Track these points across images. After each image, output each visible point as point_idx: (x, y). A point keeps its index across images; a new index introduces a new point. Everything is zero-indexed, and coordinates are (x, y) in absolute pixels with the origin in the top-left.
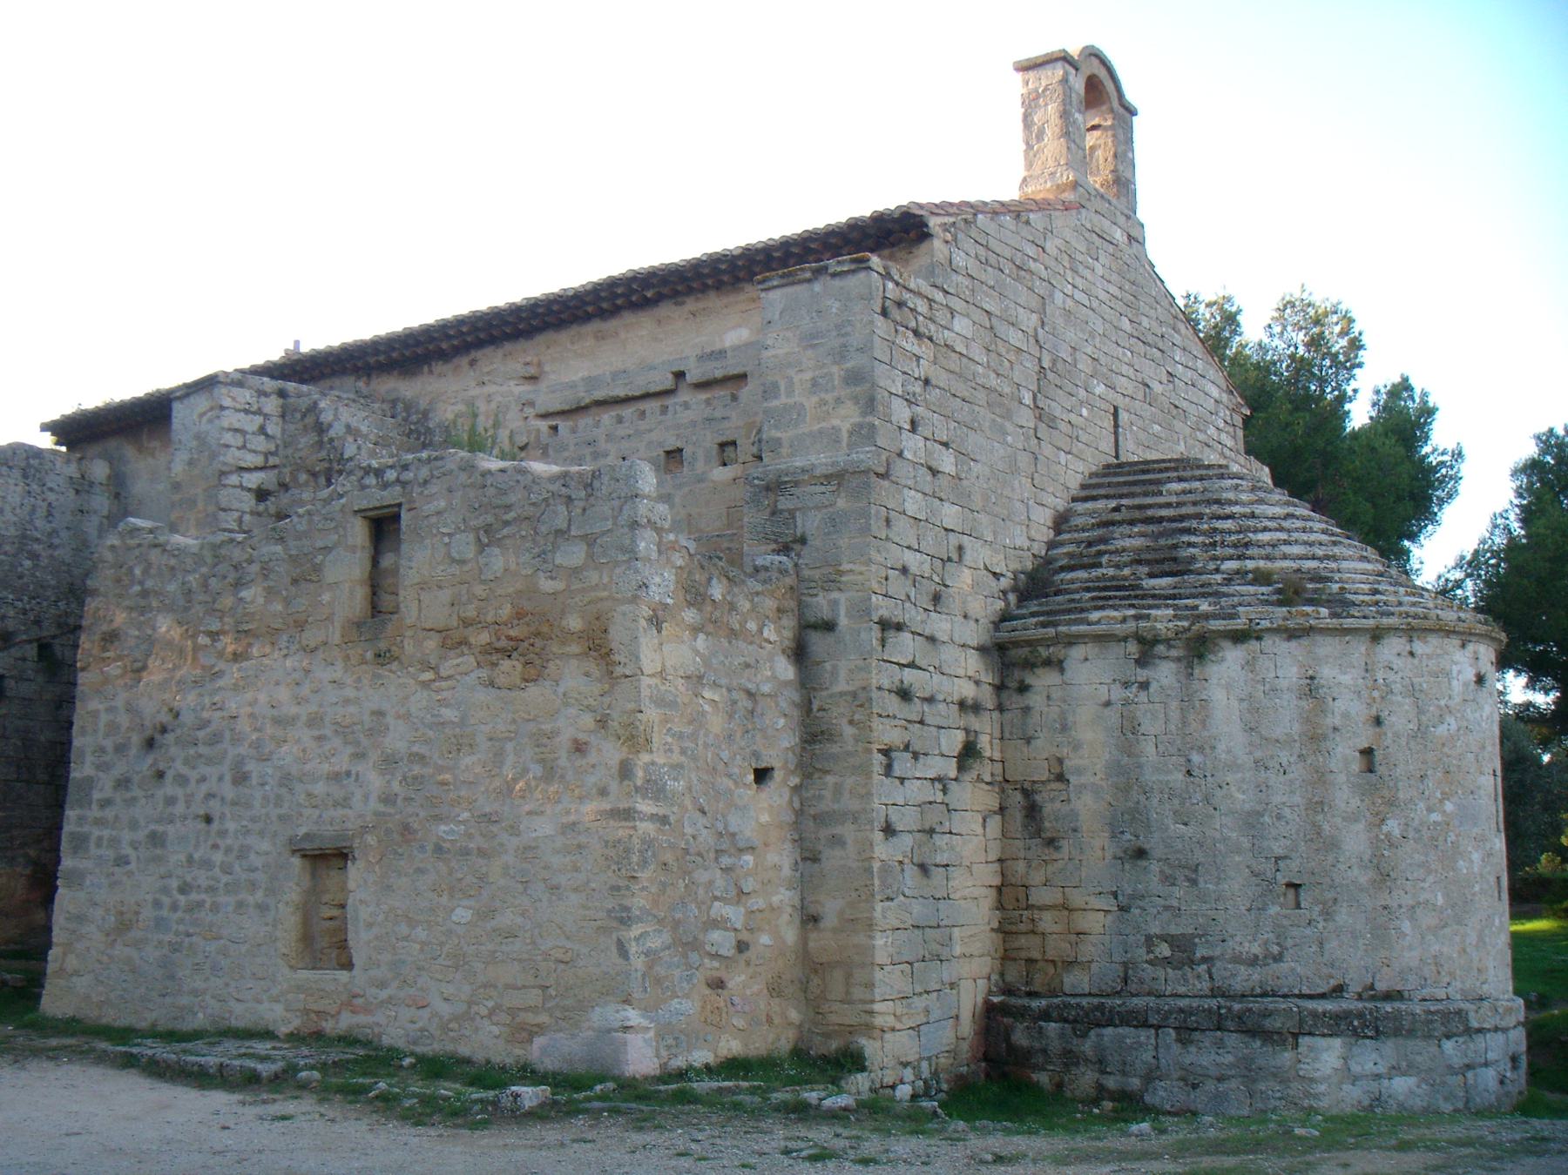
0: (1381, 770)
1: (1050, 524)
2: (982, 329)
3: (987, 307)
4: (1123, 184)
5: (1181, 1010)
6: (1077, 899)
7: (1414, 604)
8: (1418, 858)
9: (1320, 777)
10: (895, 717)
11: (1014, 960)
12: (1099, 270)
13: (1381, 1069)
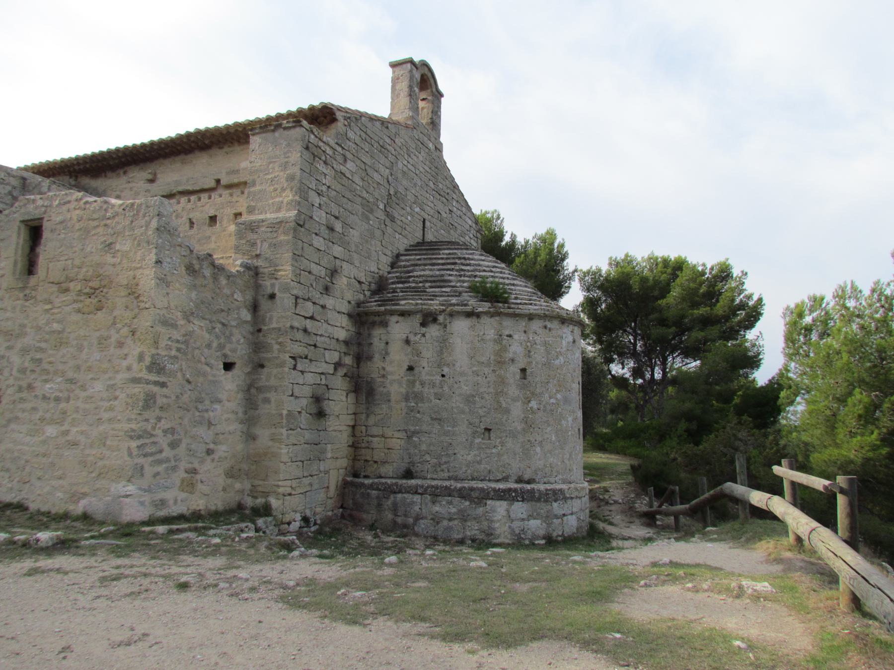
0: (529, 378)
1: (389, 263)
2: (360, 170)
3: (364, 161)
4: (435, 124)
5: (433, 487)
6: (389, 432)
7: (547, 306)
8: (545, 419)
9: (502, 381)
10: (300, 342)
11: (359, 460)
12: (421, 158)
13: (524, 516)
